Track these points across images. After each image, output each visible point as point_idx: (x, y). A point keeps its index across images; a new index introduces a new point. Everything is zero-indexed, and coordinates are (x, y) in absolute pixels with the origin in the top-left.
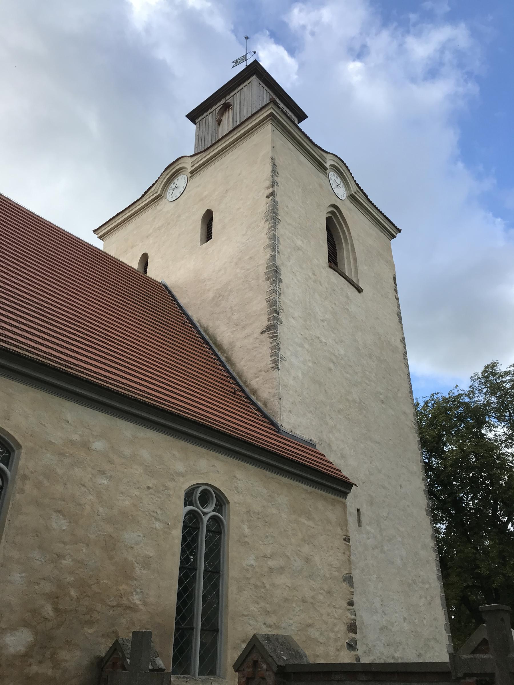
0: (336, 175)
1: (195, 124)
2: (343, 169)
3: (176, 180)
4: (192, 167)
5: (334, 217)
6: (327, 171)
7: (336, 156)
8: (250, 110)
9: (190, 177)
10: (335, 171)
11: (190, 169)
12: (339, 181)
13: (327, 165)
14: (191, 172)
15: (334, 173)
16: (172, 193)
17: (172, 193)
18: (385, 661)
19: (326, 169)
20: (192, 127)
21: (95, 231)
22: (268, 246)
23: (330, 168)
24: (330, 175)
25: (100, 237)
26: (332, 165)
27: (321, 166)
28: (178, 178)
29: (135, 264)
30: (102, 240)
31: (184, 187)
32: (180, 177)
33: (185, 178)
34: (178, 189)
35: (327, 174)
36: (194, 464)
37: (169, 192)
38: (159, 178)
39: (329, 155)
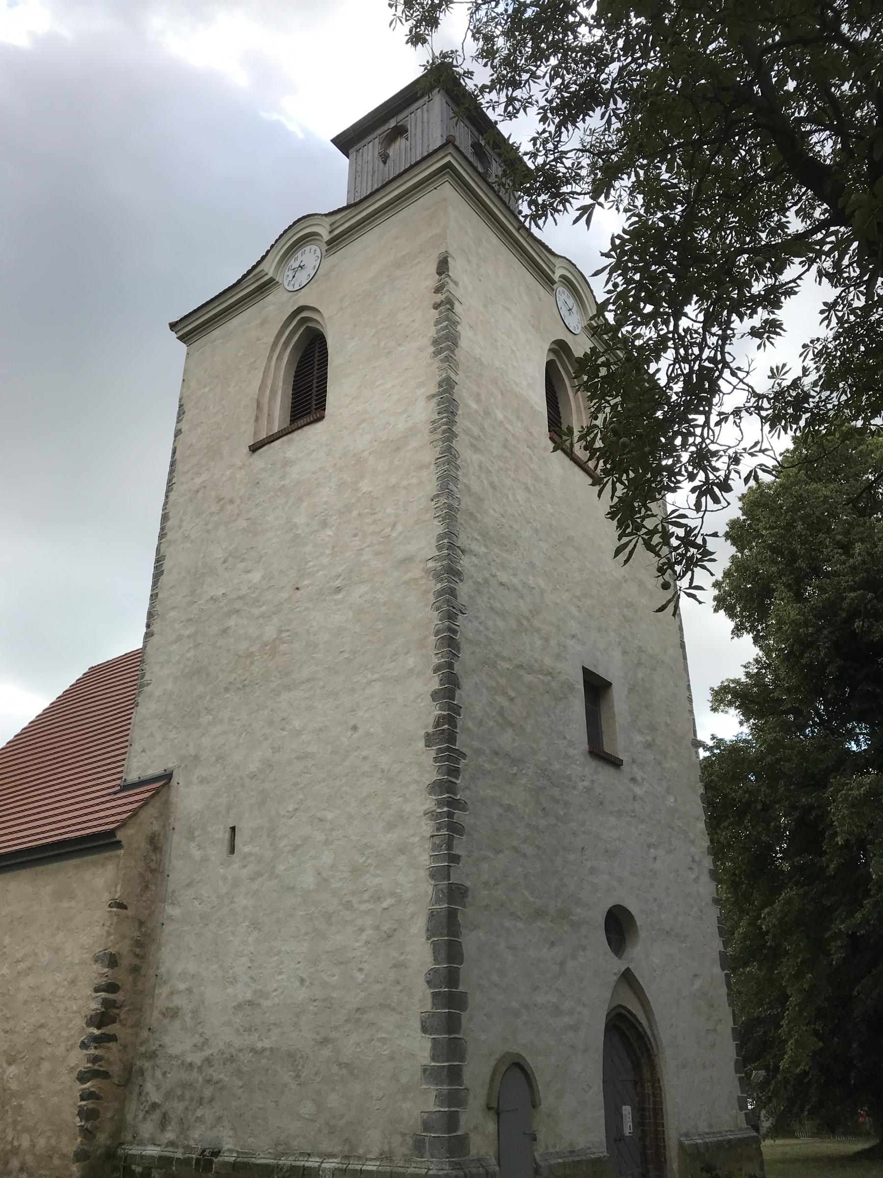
0: (566, 292)
1: (348, 157)
2: (578, 282)
3: (299, 254)
4: (331, 232)
5: (558, 359)
6: (555, 286)
7: (570, 261)
8: (426, 148)
9: (326, 251)
10: (565, 285)
11: (326, 237)
12: (571, 302)
13: (556, 277)
14: (329, 243)
15: (565, 290)
16: (294, 277)
17: (294, 277)
18: (615, 974)
19: (553, 282)
20: (343, 162)
21: (173, 326)
22: (435, 695)
23: (560, 281)
24: (557, 292)
25: (181, 338)
26: (563, 277)
27: (547, 281)
28: (303, 250)
29: (506, 137)
30: (184, 342)
31: (315, 266)
32: (307, 248)
33: (315, 251)
34: (303, 271)
35: (553, 290)
36: (285, 1033)
37: (288, 276)
38: (272, 246)
39: (560, 259)
